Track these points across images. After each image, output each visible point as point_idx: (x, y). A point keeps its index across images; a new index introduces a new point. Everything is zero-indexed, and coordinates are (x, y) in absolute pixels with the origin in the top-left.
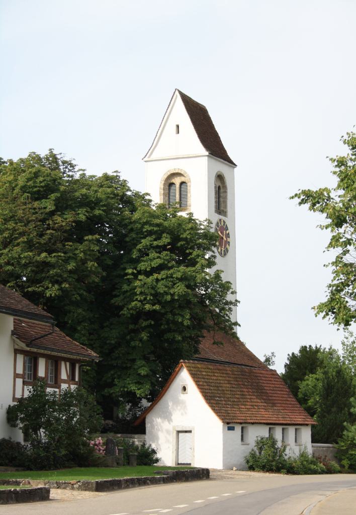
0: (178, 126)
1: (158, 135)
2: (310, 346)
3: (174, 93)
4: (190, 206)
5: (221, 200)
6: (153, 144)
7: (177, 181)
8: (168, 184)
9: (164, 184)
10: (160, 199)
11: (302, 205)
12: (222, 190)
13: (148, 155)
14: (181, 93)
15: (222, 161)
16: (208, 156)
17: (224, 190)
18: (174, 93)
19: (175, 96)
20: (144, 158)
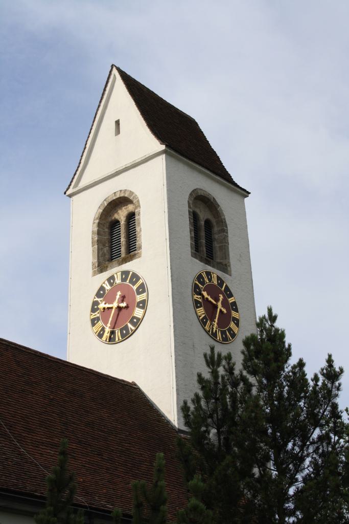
0: (118, 123)
1: (88, 146)
2: (301, 364)
3: (111, 72)
4: (140, 248)
5: (216, 245)
6: (80, 163)
7: (121, 215)
8: (108, 224)
9: (99, 224)
10: (93, 251)
11: (327, 357)
12: (216, 229)
13: (73, 184)
14: (118, 69)
15: (208, 172)
16: (164, 152)
17: (220, 228)
18: (111, 72)
19: (112, 77)
20: (67, 190)
